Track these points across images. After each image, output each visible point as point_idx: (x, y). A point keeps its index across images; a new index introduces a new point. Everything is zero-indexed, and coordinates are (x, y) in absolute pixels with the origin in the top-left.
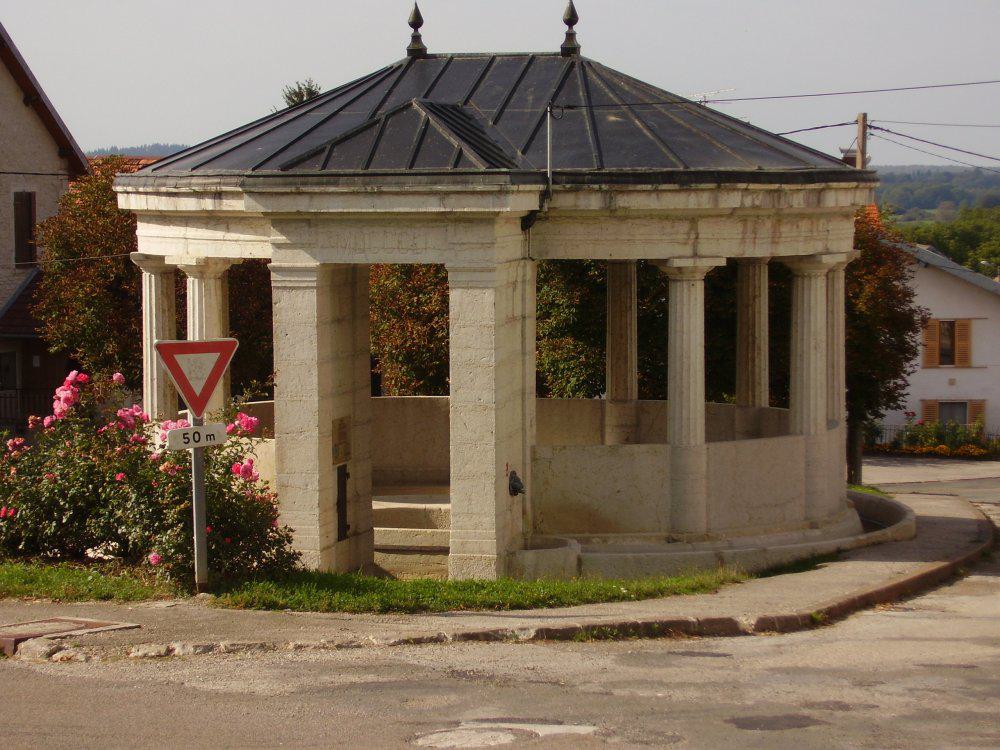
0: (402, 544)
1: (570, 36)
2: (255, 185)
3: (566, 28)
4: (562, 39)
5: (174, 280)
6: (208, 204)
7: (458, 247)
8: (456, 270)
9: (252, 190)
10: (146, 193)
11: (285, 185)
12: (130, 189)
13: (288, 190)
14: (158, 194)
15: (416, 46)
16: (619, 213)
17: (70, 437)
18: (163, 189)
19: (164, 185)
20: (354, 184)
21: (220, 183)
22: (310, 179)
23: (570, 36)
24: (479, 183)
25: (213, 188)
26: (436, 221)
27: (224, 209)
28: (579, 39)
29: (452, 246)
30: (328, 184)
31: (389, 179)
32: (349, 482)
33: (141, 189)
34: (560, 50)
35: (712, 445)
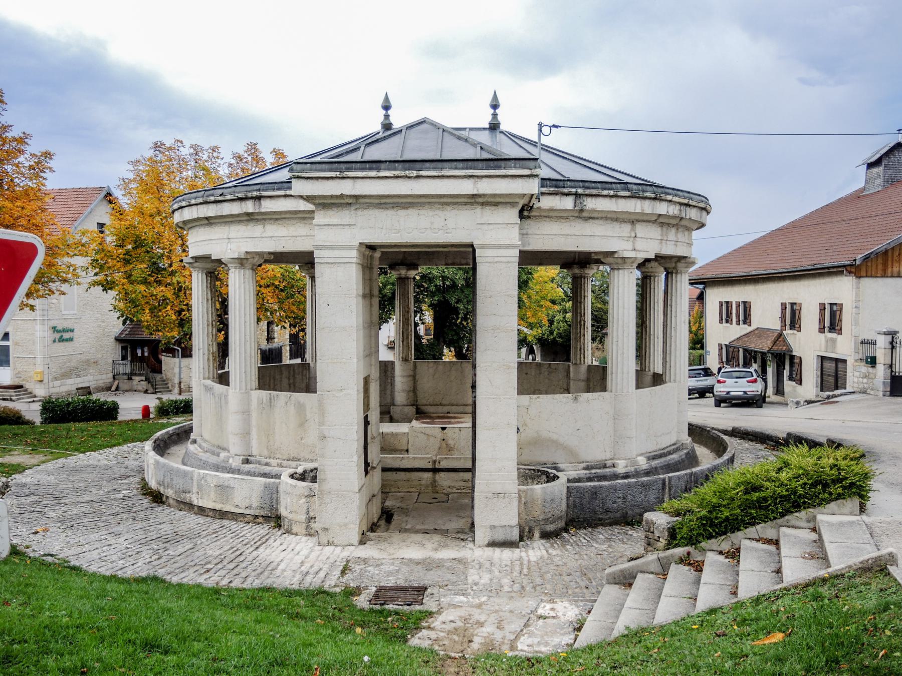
0: (355, 458)
1: (495, 116)
2: (303, 171)
3: (492, 111)
4: (490, 118)
5: (214, 271)
6: (249, 207)
7: (485, 227)
8: (483, 247)
9: (300, 174)
10: (197, 204)
11: (331, 170)
12: (184, 204)
13: (333, 174)
14: (206, 203)
15: (387, 122)
16: (585, 214)
17: (306, 606)
18: (212, 199)
19: (213, 195)
20: (395, 169)
21: (259, 190)
22: (354, 165)
23: (495, 116)
24: (511, 168)
25: (254, 194)
26: (466, 204)
27: (263, 211)
28: (499, 118)
29: (479, 226)
30: (371, 169)
31: (427, 165)
32: (369, 427)
33: (193, 202)
34: (488, 126)
35: (525, 398)
